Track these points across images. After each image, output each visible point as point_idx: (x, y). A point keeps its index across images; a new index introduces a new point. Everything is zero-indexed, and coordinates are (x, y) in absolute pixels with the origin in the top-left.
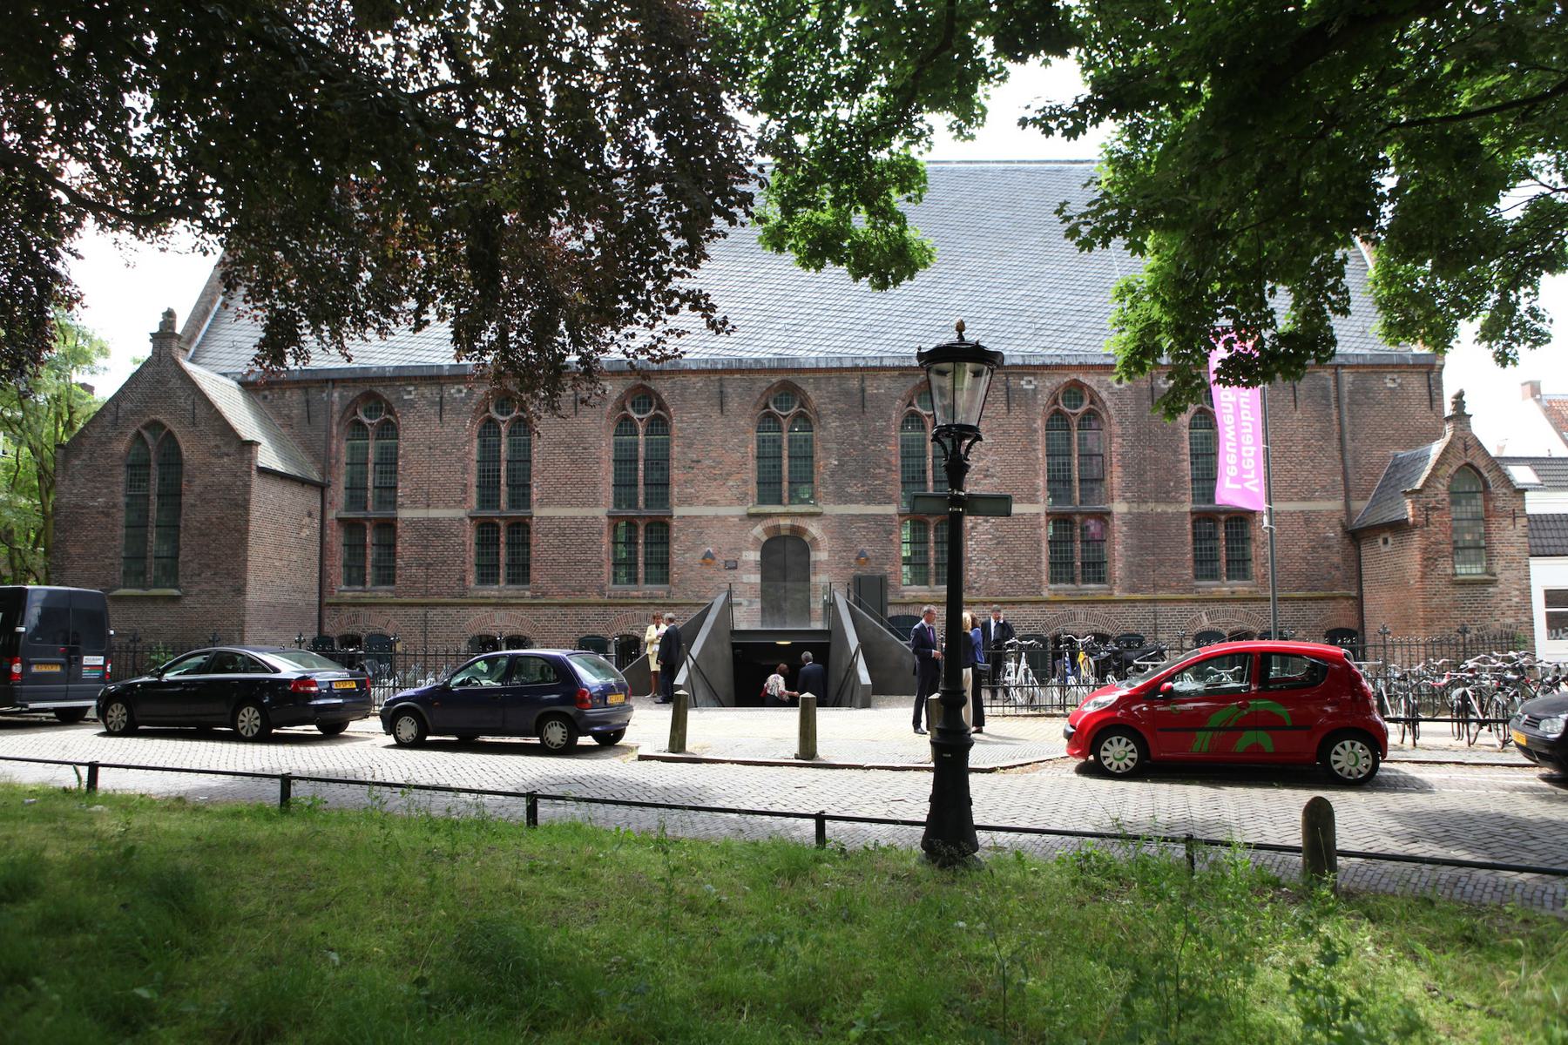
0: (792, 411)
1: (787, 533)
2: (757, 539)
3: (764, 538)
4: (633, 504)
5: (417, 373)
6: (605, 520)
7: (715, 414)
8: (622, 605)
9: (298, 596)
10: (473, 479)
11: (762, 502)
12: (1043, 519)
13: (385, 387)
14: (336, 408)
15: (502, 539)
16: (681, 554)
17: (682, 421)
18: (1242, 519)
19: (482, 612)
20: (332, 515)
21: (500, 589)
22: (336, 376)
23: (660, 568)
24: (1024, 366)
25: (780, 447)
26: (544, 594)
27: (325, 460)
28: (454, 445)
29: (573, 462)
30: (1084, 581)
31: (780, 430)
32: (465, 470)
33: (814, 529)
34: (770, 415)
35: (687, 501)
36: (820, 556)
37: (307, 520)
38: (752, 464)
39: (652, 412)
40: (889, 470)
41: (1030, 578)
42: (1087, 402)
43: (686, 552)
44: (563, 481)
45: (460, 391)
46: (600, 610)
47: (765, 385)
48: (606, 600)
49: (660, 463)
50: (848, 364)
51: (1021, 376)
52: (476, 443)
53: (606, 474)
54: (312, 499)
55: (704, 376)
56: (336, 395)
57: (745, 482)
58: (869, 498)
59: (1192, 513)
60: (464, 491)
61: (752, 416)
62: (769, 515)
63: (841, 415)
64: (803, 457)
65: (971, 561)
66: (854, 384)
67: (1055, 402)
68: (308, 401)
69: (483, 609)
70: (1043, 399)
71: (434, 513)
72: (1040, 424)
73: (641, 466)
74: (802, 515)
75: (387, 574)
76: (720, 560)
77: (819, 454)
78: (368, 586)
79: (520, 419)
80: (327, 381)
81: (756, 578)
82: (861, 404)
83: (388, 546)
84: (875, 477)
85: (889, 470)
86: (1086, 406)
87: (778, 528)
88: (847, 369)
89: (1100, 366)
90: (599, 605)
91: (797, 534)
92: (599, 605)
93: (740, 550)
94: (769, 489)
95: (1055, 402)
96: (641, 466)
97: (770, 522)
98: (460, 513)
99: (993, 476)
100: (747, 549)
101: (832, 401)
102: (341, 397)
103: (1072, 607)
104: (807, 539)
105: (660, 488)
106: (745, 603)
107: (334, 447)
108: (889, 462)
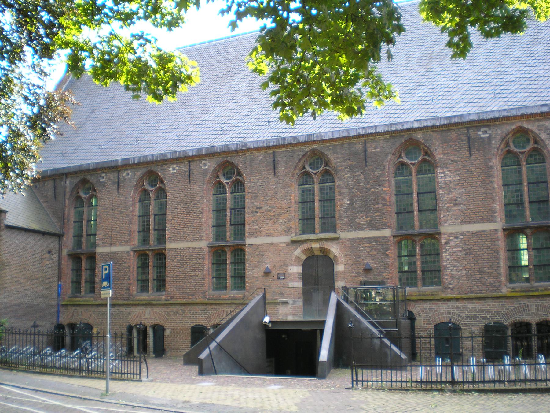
0: (321, 169)
1: (318, 253)
2: (298, 258)
3: (304, 257)
4: (224, 238)
5: (106, 165)
6: (206, 249)
7: (271, 176)
8: (216, 304)
9: (38, 300)
10: (136, 227)
11: (304, 233)
12: (500, 234)
13: (91, 175)
14: (68, 189)
15: (151, 264)
16: (253, 271)
17: (250, 182)
18: (216, 252)
19: (139, 309)
20: (65, 252)
21: (151, 295)
22: (66, 171)
23: (240, 279)
24: (479, 121)
25: (314, 194)
26: (172, 298)
27: (62, 219)
28: (125, 207)
29: (188, 213)
30: (424, 285)
31: (411, 174)
32: (131, 222)
33: (334, 249)
34: (306, 174)
35: (254, 234)
36: (340, 268)
37: (47, 255)
38: (294, 207)
39: (234, 178)
40: (384, 205)
41: (492, 279)
42: (532, 142)
43: (253, 268)
44: (182, 225)
45: (128, 174)
46: (203, 308)
47: (301, 153)
48: (206, 301)
49: (239, 209)
50: (352, 134)
51: (478, 128)
52: (138, 205)
53: (208, 219)
54: (53, 244)
55: (262, 152)
56: (68, 182)
57: (290, 220)
58: (371, 226)
59: (504, 230)
60: (130, 235)
61: (293, 176)
62: (305, 241)
63: (351, 168)
64: (329, 200)
65: (446, 268)
66: (359, 147)
67: (507, 145)
68: (55, 187)
69: (139, 308)
70: (495, 143)
71: (115, 249)
72: (496, 163)
73: (228, 213)
74: (326, 240)
75: (161, 284)
76: (274, 272)
77: (338, 197)
78: (83, 293)
79: (160, 187)
80: (63, 174)
81: (299, 285)
82: (364, 160)
83: (161, 265)
84: (375, 210)
85: (384, 205)
86: (531, 145)
87: (311, 249)
88: (353, 137)
89: (537, 114)
90: (203, 304)
91: (325, 253)
92: (203, 304)
93: (287, 266)
94: (307, 223)
95: (507, 145)
96: (228, 213)
97: (305, 246)
98: (127, 248)
99: (460, 204)
100: (292, 265)
101: (345, 160)
102: (70, 183)
103: (526, 301)
104: (332, 257)
105: (240, 226)
106: (291, 302)
107: (66, 212)
108: (384, 199)
